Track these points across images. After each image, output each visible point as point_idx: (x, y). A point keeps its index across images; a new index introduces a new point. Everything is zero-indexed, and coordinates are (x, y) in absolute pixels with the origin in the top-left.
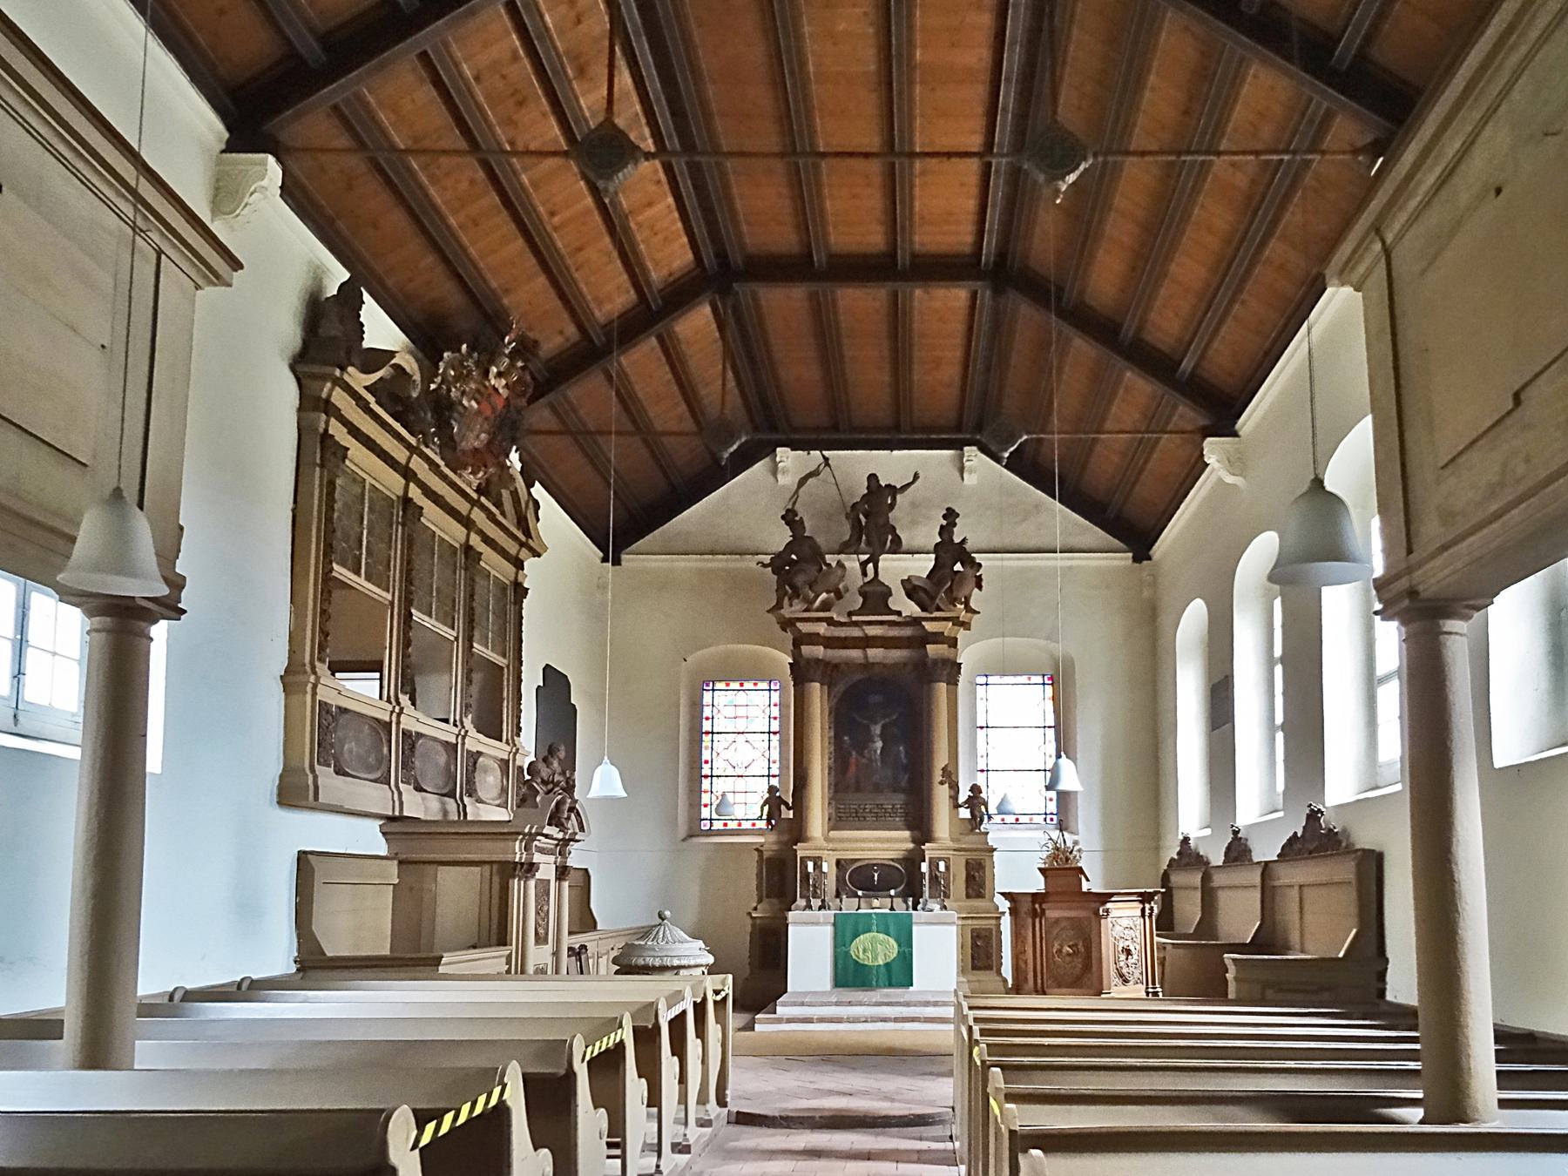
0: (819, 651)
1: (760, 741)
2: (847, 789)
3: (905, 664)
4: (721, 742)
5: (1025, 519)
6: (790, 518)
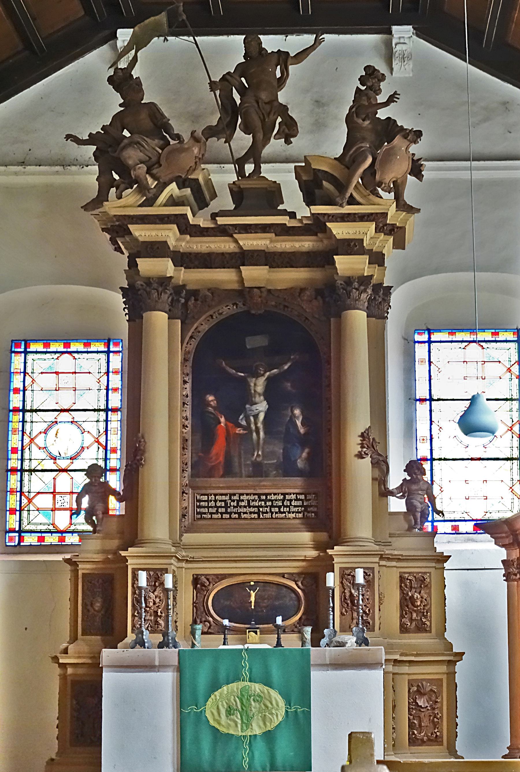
0: (166, 267)
1: (92, 424)
2: (210, 473)
3: (302, 290)
5: (486, 119)
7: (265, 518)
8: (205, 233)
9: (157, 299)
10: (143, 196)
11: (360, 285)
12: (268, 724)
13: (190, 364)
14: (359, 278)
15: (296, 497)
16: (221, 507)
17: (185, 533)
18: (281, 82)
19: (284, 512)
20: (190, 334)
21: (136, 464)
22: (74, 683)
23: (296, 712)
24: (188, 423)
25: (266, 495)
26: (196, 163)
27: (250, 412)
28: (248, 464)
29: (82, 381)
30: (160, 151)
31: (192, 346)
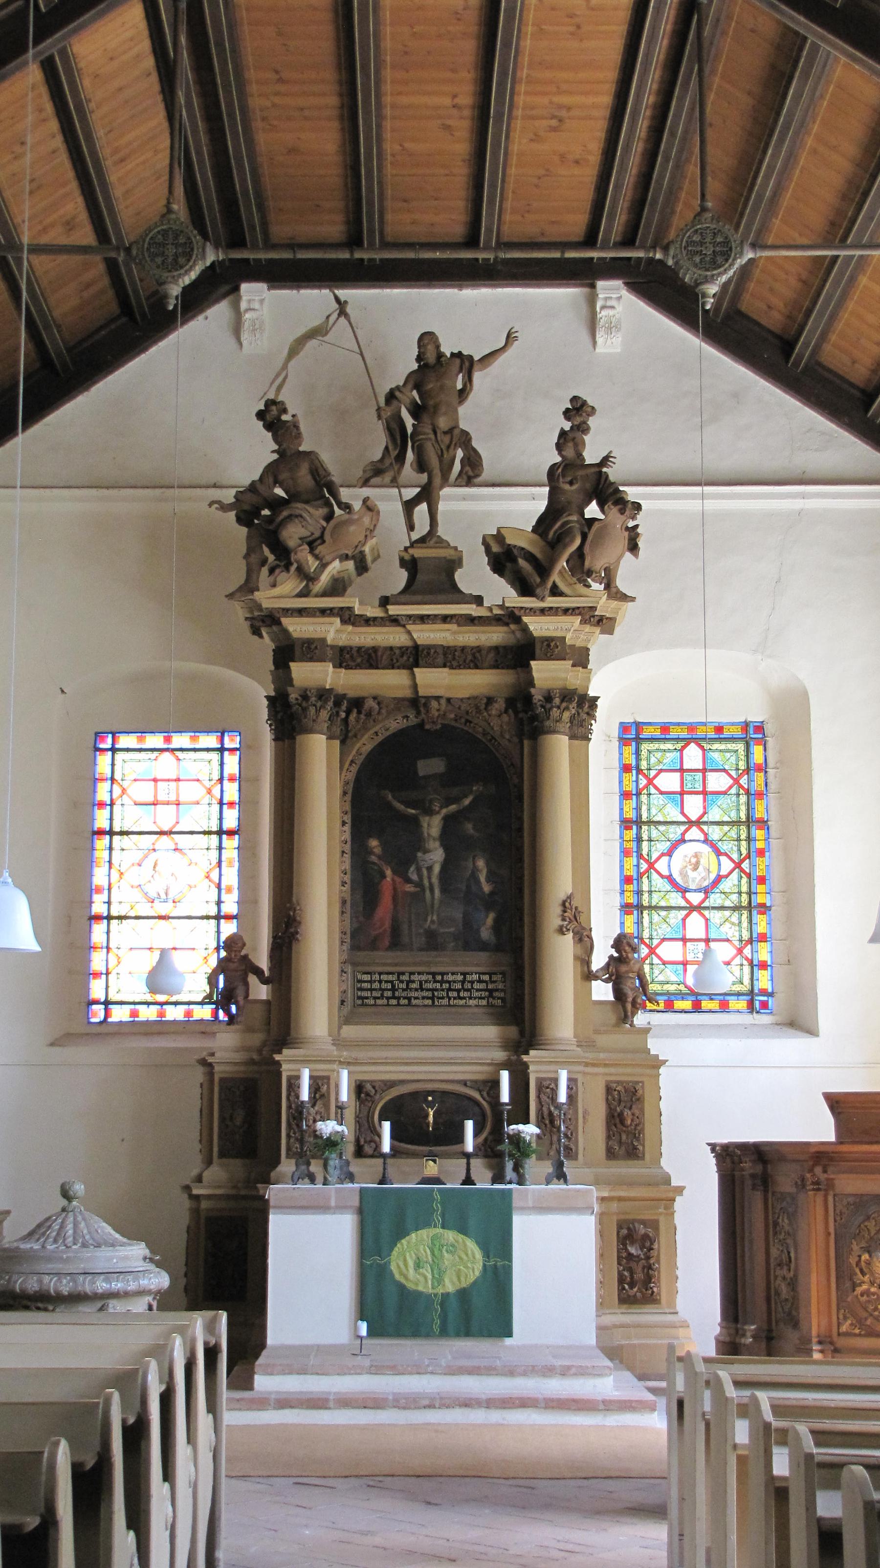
1: (202, 850)
2: (373, 945)
3: (490, 700)
4: (127, 851)
6: (272, 417)
8: (372, 623)
11: (562, 701)
12: (463, 1279)
13: (348, 798)
15: (479, 977)
17: (345, 1024)
18: (463, 394)
19: (464, 998)
20: (350, 758)
21: (289, 937)
22: (210, 1220)
23: (495, 1266)
24: (347, 878)
25: (443, 974)
26: (366, 536)
31: (351, 776)
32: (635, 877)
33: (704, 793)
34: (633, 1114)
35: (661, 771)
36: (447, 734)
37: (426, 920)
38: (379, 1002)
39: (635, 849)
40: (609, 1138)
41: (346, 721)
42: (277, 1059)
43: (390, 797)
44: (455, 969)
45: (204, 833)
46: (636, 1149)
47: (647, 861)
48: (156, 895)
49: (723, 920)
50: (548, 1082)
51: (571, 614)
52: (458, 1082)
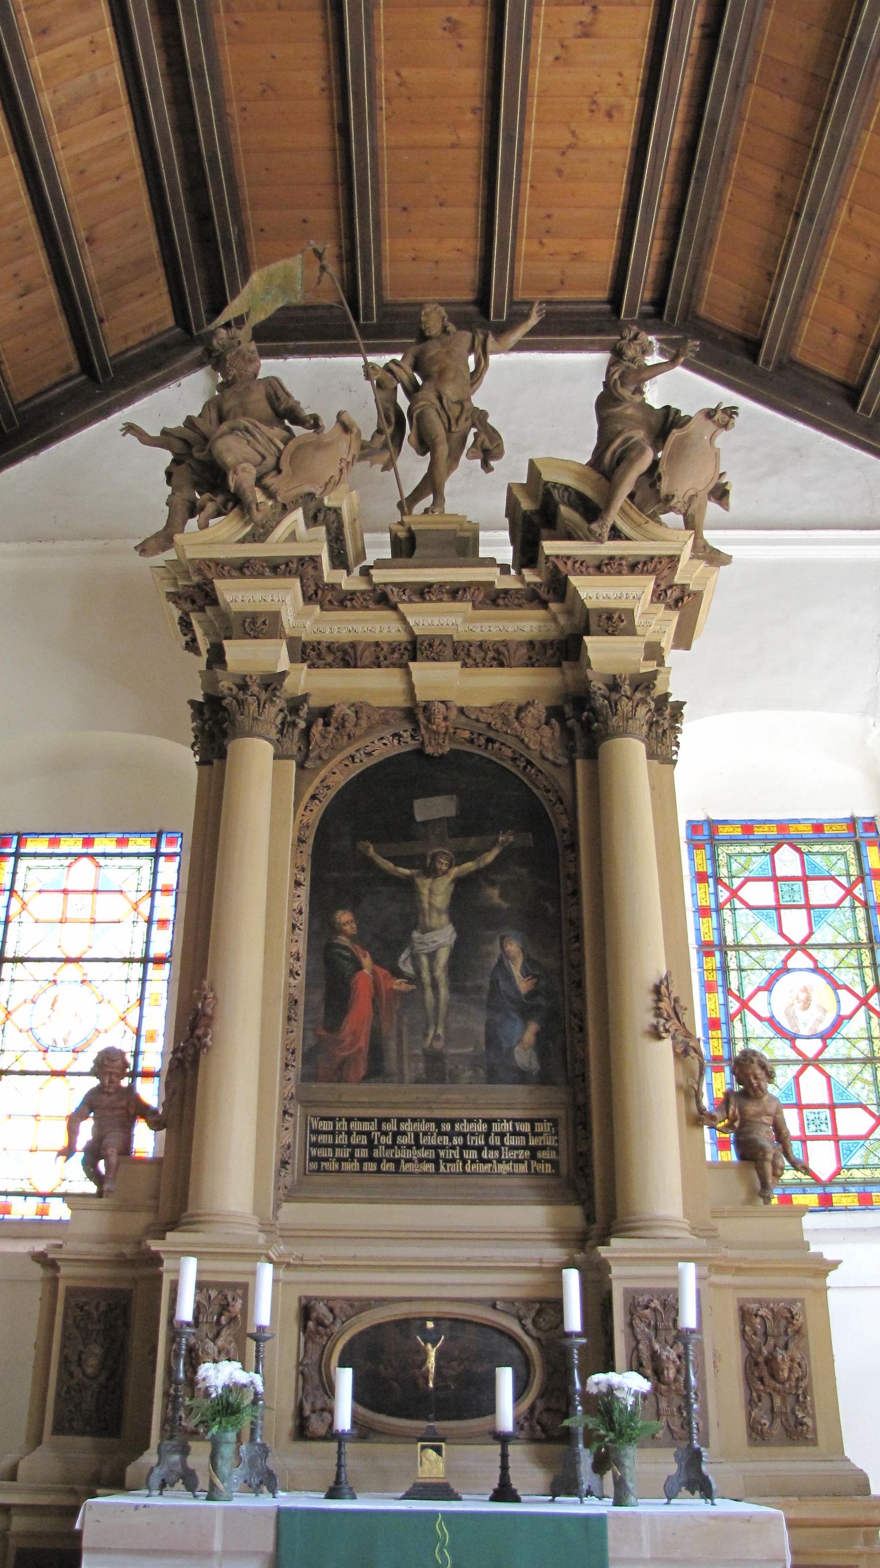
2: (339, 1074)
7: (451, 1173)
8: (348, 603)
9: (256, 715)
10: (247, 524)
13: (308, 848)
14: (632, 677)
15: (514, 1127)
16: (360, 1146)
17: (286, 1201)
18: (476, 376)
19: (489, 1161)
20: (310, 791)
24: (301, 967)
25: (453, 1122)
26: (341, 470)
27: (421, 947)
28: (416, 1055)
29: (108, 907)
30: (282, 446)
31: (314, 817)
32: (723, 1020)
33: (808, 907)
34: (792, 1360)
35: (747, 880)
36: (456, 761)
37: (426, 1035)
38: (347, 1166)
39: (720, 983)
40: (751, 1403)
41: (306, 734)
42: (153, 1248)
43: (371, 850)
44: (472, 1114)
45: (125, 960)
46: (802, 1424)
47: (738, 999)
48: (51, 1043)
49: (851, 1078)
50: (646, 1298)
51: (642, 573)
52: (479, 1301)
